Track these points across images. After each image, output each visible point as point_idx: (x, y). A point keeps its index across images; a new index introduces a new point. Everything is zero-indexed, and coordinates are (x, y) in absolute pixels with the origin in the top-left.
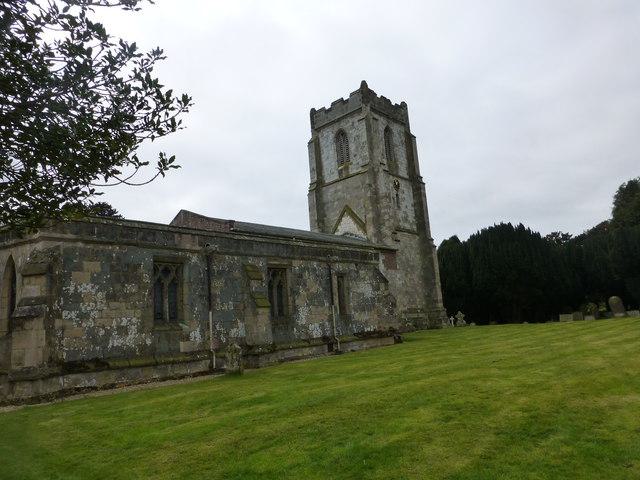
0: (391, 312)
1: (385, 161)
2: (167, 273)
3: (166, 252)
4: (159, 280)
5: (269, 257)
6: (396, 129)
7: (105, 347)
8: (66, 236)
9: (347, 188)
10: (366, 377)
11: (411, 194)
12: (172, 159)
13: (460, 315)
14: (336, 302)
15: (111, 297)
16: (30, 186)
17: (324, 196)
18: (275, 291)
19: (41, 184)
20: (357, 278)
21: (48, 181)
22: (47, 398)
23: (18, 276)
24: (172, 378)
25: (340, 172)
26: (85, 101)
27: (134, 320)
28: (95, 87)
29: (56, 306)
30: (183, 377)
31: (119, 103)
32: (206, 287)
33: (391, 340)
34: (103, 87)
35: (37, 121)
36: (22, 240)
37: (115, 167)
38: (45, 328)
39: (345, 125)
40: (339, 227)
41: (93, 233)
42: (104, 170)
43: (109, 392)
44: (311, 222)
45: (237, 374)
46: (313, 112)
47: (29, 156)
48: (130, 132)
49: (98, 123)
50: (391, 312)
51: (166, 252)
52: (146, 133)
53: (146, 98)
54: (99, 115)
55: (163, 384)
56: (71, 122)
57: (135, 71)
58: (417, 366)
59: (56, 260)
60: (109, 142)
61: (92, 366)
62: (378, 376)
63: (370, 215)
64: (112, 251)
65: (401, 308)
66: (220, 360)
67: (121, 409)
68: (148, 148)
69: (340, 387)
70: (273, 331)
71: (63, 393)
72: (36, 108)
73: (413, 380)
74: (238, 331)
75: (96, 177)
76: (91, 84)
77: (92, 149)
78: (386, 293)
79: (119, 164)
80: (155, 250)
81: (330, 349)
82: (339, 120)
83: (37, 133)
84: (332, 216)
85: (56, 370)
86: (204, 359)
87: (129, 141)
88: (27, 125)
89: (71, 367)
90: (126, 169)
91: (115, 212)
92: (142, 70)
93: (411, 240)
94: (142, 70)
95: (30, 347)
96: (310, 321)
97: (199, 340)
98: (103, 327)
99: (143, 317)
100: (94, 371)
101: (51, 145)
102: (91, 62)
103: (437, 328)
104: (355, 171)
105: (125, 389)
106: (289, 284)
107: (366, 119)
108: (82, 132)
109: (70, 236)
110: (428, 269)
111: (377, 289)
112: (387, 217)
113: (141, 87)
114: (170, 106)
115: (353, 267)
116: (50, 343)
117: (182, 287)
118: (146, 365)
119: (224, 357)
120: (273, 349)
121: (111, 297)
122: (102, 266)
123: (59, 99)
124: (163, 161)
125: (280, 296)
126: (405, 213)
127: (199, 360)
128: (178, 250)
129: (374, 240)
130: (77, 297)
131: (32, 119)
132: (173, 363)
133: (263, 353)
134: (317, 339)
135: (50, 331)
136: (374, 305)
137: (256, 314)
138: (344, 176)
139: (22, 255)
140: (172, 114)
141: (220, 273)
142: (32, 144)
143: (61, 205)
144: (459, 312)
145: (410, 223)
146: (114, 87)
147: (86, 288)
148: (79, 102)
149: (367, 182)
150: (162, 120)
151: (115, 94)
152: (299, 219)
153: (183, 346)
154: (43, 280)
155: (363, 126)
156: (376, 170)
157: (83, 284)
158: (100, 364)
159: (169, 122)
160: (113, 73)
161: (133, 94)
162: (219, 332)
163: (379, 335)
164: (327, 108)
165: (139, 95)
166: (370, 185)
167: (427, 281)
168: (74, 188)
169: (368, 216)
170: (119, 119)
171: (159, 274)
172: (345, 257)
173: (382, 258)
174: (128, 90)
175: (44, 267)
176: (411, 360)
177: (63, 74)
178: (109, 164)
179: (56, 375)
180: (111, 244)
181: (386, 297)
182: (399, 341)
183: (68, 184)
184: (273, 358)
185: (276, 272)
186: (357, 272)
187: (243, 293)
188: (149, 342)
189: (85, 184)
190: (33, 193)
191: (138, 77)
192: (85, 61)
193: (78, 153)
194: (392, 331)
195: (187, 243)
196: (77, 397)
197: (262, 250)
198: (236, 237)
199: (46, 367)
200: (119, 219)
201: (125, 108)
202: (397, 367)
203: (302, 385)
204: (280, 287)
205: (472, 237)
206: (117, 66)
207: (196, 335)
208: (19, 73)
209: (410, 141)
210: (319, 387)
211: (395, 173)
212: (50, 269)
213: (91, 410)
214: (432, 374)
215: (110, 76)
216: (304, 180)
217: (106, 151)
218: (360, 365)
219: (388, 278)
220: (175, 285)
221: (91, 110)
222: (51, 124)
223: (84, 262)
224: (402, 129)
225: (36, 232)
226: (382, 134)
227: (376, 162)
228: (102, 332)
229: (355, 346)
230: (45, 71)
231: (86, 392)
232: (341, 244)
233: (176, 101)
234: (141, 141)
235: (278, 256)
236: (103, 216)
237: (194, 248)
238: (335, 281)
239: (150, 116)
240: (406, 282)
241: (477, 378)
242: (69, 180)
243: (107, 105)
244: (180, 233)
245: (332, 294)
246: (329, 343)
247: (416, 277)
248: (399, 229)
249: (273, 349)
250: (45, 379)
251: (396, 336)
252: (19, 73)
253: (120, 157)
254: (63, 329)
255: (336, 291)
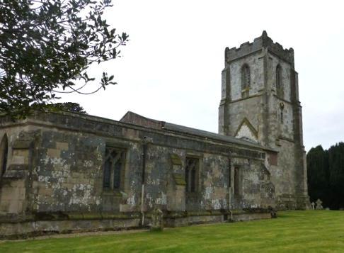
0: (271, 196)
1: (275, 89)
2: (115, 155)
3: (116, 140)
4: (109, 159)
5: (187, 150)
6: (285, 66)
7: (67, 204)
8: (45, 123)
9: (247, 105)
10: (249, 240)
11: (292, 114)
12: (112, 78)
13: (319, 202)
14: (233, 185)
15: (74, 169)
16: (10, 89)
17: (230, 110)
18: (190, 174)
19: (18, 88)
20: (249, 170)
21: (22, 86)
22: (23, 236)
23: (10, 149)
24: (112, 230)
25: (243, 94)
26: (53, 31)
27: (89, 186)
28: (61, 22)
29: (34, 172)
30: (120, 229)
31: (77, 35)
32: (142, 167)
33: (269, 215)
34: (67, 23)
35: (19, 42)
36: (14, 124)
37: (71, 80)
38: (26, 187)
39: (249, 61)
40: (239, 133)
41: (65, 123)
42: (63, 82)
43: (67, 236)
44: (219, 127)
45: (158, 230)
46: (227, 49)
47: (10, 67)
48: (84, 56)
49: (62, 48)
50: (271, 196)
51: (116, 140)
52: (95, 58)
53: (97, 33)
54: (63, 42)
55: (105, 233)
56: (42, 46)
57: (90, 13)
58: (286, 236)
59: (37, 139)
60: (68, 62)
61: (56, 216)
62: (257, 240)
63: (261, 126)
64: (77, 136)
65: (278, 194)
66: (147, 220)
67: (74, 248)
68: (95, 69)
69: (231, 245)
70: (186, 202)
71: (35, 234)
72: (19, 34)
73: (283, 245)
74: (162, 200)
75: (56, 86)
76: (58, 20)
77: (56, 66)
78: (268, 182)
79: (73, 78)
80: (108, 138)
81: (226, 218)
82: (245, 57)
83: (17, 51)
84: (235, 125)
85: (31, 217)
86: (136, 218)
87: (82, 62)
88: (11, 45)
89: (42, 216)
90: (78, 82)
91: (81, 109)
92: (95, 13)
93: (289, 146)
94: (95, 13)
95: (14, 199)
96: (213, 197)
97: (133, 204)
98: (67, 189)
99: (95, 185)
100: (59, 220)
101: (26, 61)
102: (60, 4)
103: (303, 210)
104: (254, 94)
105: (79, 235)
106: (200, 170)
107: (264, 58)
108: (49, 53)
109: (48, 123)
110: (299, 167)
111: (262, 178)
112: (273, 128)
113: (94, 25)
114: (113, 40)
115: (246, 161)
116: (28, 198)
117: (125, 165)
118: (95, 219)
119: (150, 218)
120: (185, 215)
121: (74, 169)
122: (69, 146)
123: (35, 29)
124: (105, 79)
125: (193, 178)
126: (286, 126)
127: (132, 218)
128: (123, 139)
129: (263, 144)
130: (50, 167)
131: (15, 41)
132: (114, 219)
133: (178, 217)
134: (218, 210)
135: (29, 189)
136: (259, 190)
137: (175, 189)
138: (245, 96)
139: (14, 134)
140: (114, 46)
141: (153, 158)
142: (14, 59)
143: (30, 104)
144: (319, 200)
145: (289, 134)
146: (74, 23)
147: (57, 161)
148: (49, 32)
149: (261, 102)
150: (106, 49)
151: (75, 28)
152: (209, 123)
153: (122, 208)
154: (27, 153)
155: (261, 63)
156: (268, 94)
157: (55, 158)
158: (62, 216)
159: (112, 52)
160: (75, 13)
161: (88, 29)
162: (148, 200)
163: (260, 211)
164: (237, 48)
165: (92, 31)
166: (263, 105)
167: (298, 176)
168: (41, 92)
169: (260, 127)
170: (76, 46)
171: (109, 155)
172: (241, 154)
173: (267, 156)
174: (84, 26)
175: (28, 143)
176: (282, 231)
177: (40, 11)
178: (67, 77)
179: (31, 221)
180: (77, 131)
181: (268, 184)
182: (274, 216)
183: (37, 90)
184: (184, 221)
185: (192, 161)
186: (249, 165)
187: (167, 174)
188: (98, 203)
189: (49, 90)
190: (11, 93)
191: (92, 17)
192: (56, 3)
193: (46, 68)
194: (270, 209)
195: (131, 135)
196: (44, 237)
197: (183, 144)
198: (166, 134)
199: (24, 214)
200: (84, 114)
201: (81, 39)
202: (272, 235)
203: (204, 242)
204: (194, 172)
205: (332, 147)
206: (78, 9)
207: (132, 201)
208: (8, 8)
209: (294, 76)
210: (216, 244)
211: (281, 97)
212: (32, 146)
213: (52, 247)
214: (295, 241)
215: (73, 15)
216: (217, 96)
217: (65, 69)
218: (245, 231)
219: (270, 171)
220: (120, 164)
221: (57, 38)
222: (28, 46)
223: (57, 143)
224: (289, 67)
225: (25, 118)
226: (274, 70)
227: (268, 89)
228: (65, 193)
229: (244, 217)
230: (27, 7)
231: (51, 234)
232: (239, 145)
233: (117, 37)
234: (91, 63)
235: (194, 150)
236: (73, 111)
237: (136, 139)
238: (233, 170)
239: (99, 46)
240: (283, 176)
241: (327, 247)
242: (38, 86)
243: (69, 35)
244: (127, 128)
245: (230, 180)
246: (225, 214)
247: (290, 173)
248: (280, 138)
249: (185, 215)
250: (22, 222)
251: (272, 213)
252: (8, 8)
253: (75, 73)
254: (38, 188)
255: (233, 177)
